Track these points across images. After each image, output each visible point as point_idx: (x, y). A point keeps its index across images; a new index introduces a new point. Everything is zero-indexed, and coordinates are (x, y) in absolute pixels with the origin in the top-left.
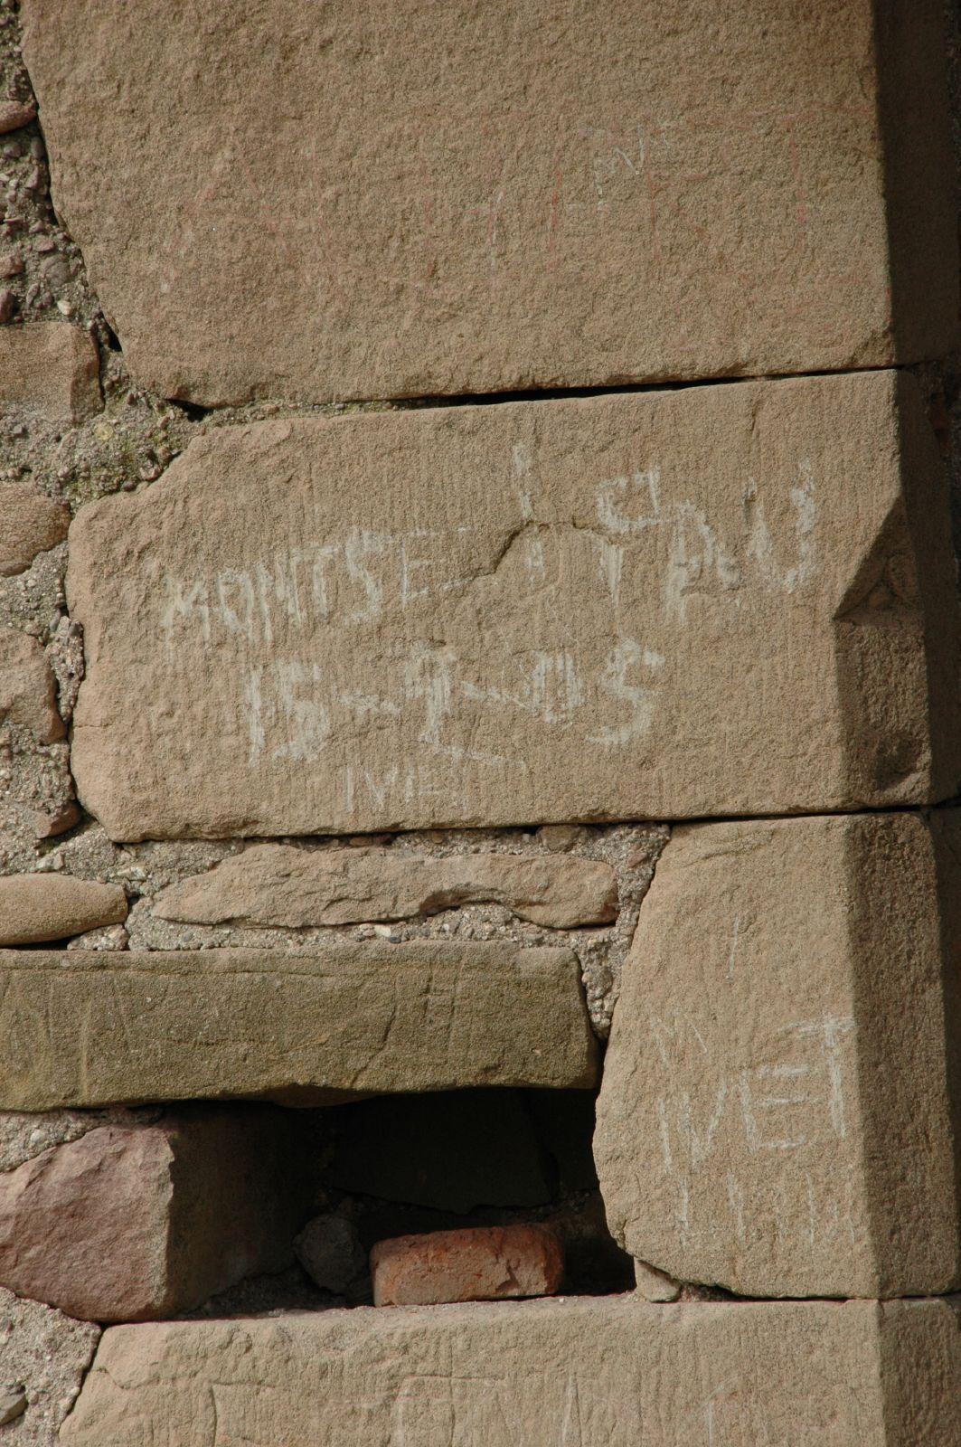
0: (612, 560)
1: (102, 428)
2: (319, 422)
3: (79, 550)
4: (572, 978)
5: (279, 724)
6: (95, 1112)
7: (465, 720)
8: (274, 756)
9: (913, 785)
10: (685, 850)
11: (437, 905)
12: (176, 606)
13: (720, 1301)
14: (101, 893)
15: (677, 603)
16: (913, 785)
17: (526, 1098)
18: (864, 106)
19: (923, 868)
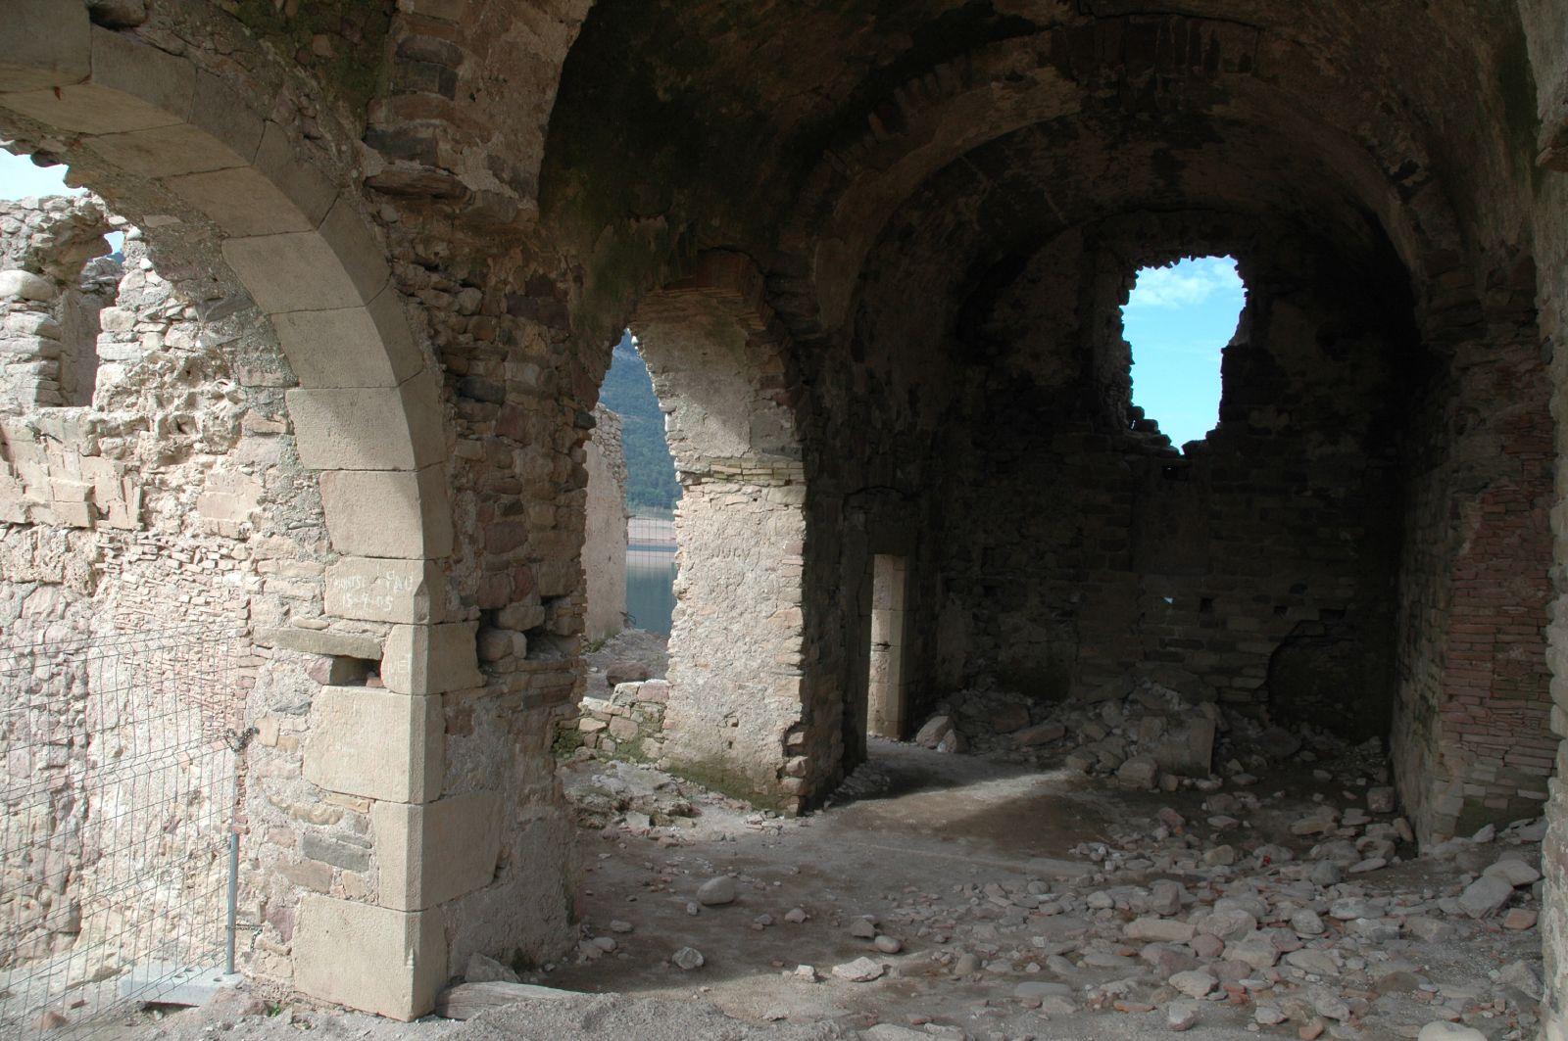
0: (388, 583)
1: (330, 556)
2: (355, 559)
3: (326, 573)
4: (379, 644)
5: (347, 602)
6: (325, 655)
7: (369, 604)
8: (1284, 420)
9: (426, 621)
10: (396, 627)
11: (364, 631)
12: (336, 583)
13: (1230, 341)
14: (325, 624)
15: (395, 591)
16: (426, 621)
17: (373, 661)
18: (420, 522)
19: (426, 634)
